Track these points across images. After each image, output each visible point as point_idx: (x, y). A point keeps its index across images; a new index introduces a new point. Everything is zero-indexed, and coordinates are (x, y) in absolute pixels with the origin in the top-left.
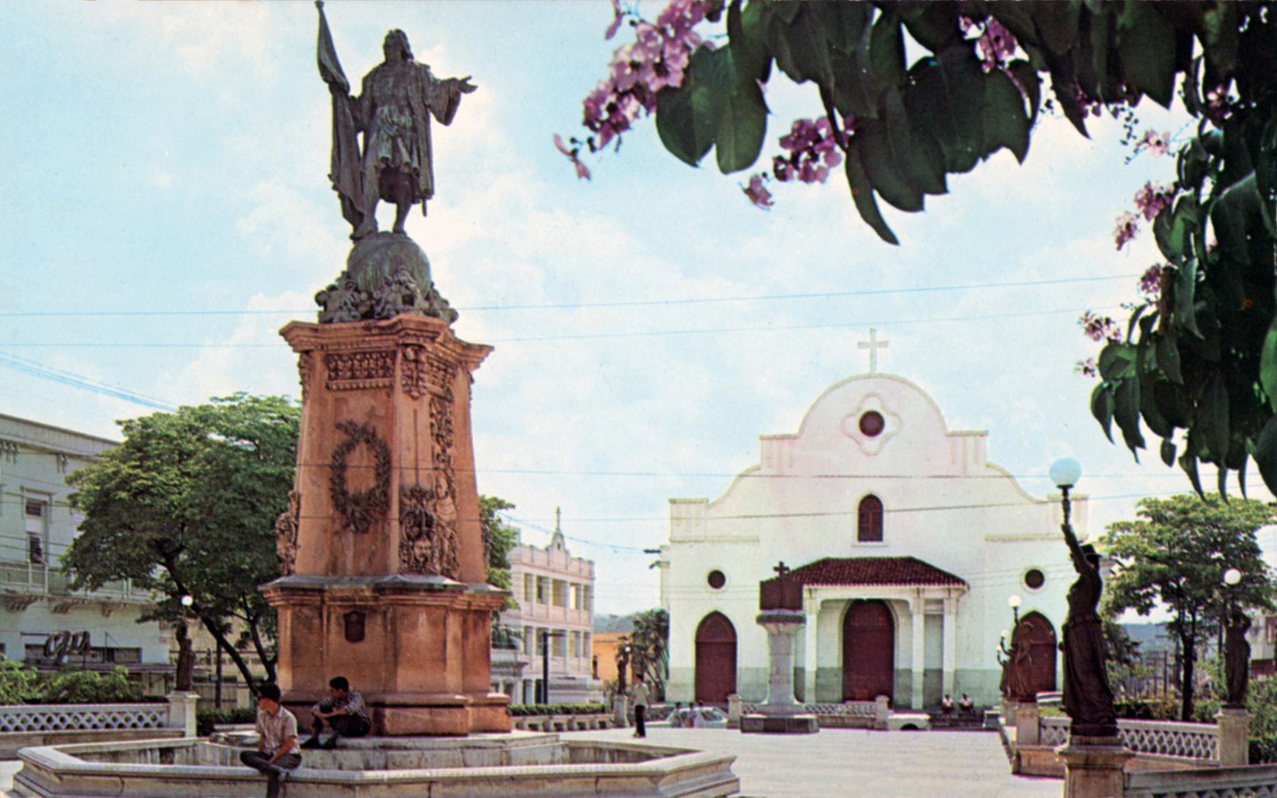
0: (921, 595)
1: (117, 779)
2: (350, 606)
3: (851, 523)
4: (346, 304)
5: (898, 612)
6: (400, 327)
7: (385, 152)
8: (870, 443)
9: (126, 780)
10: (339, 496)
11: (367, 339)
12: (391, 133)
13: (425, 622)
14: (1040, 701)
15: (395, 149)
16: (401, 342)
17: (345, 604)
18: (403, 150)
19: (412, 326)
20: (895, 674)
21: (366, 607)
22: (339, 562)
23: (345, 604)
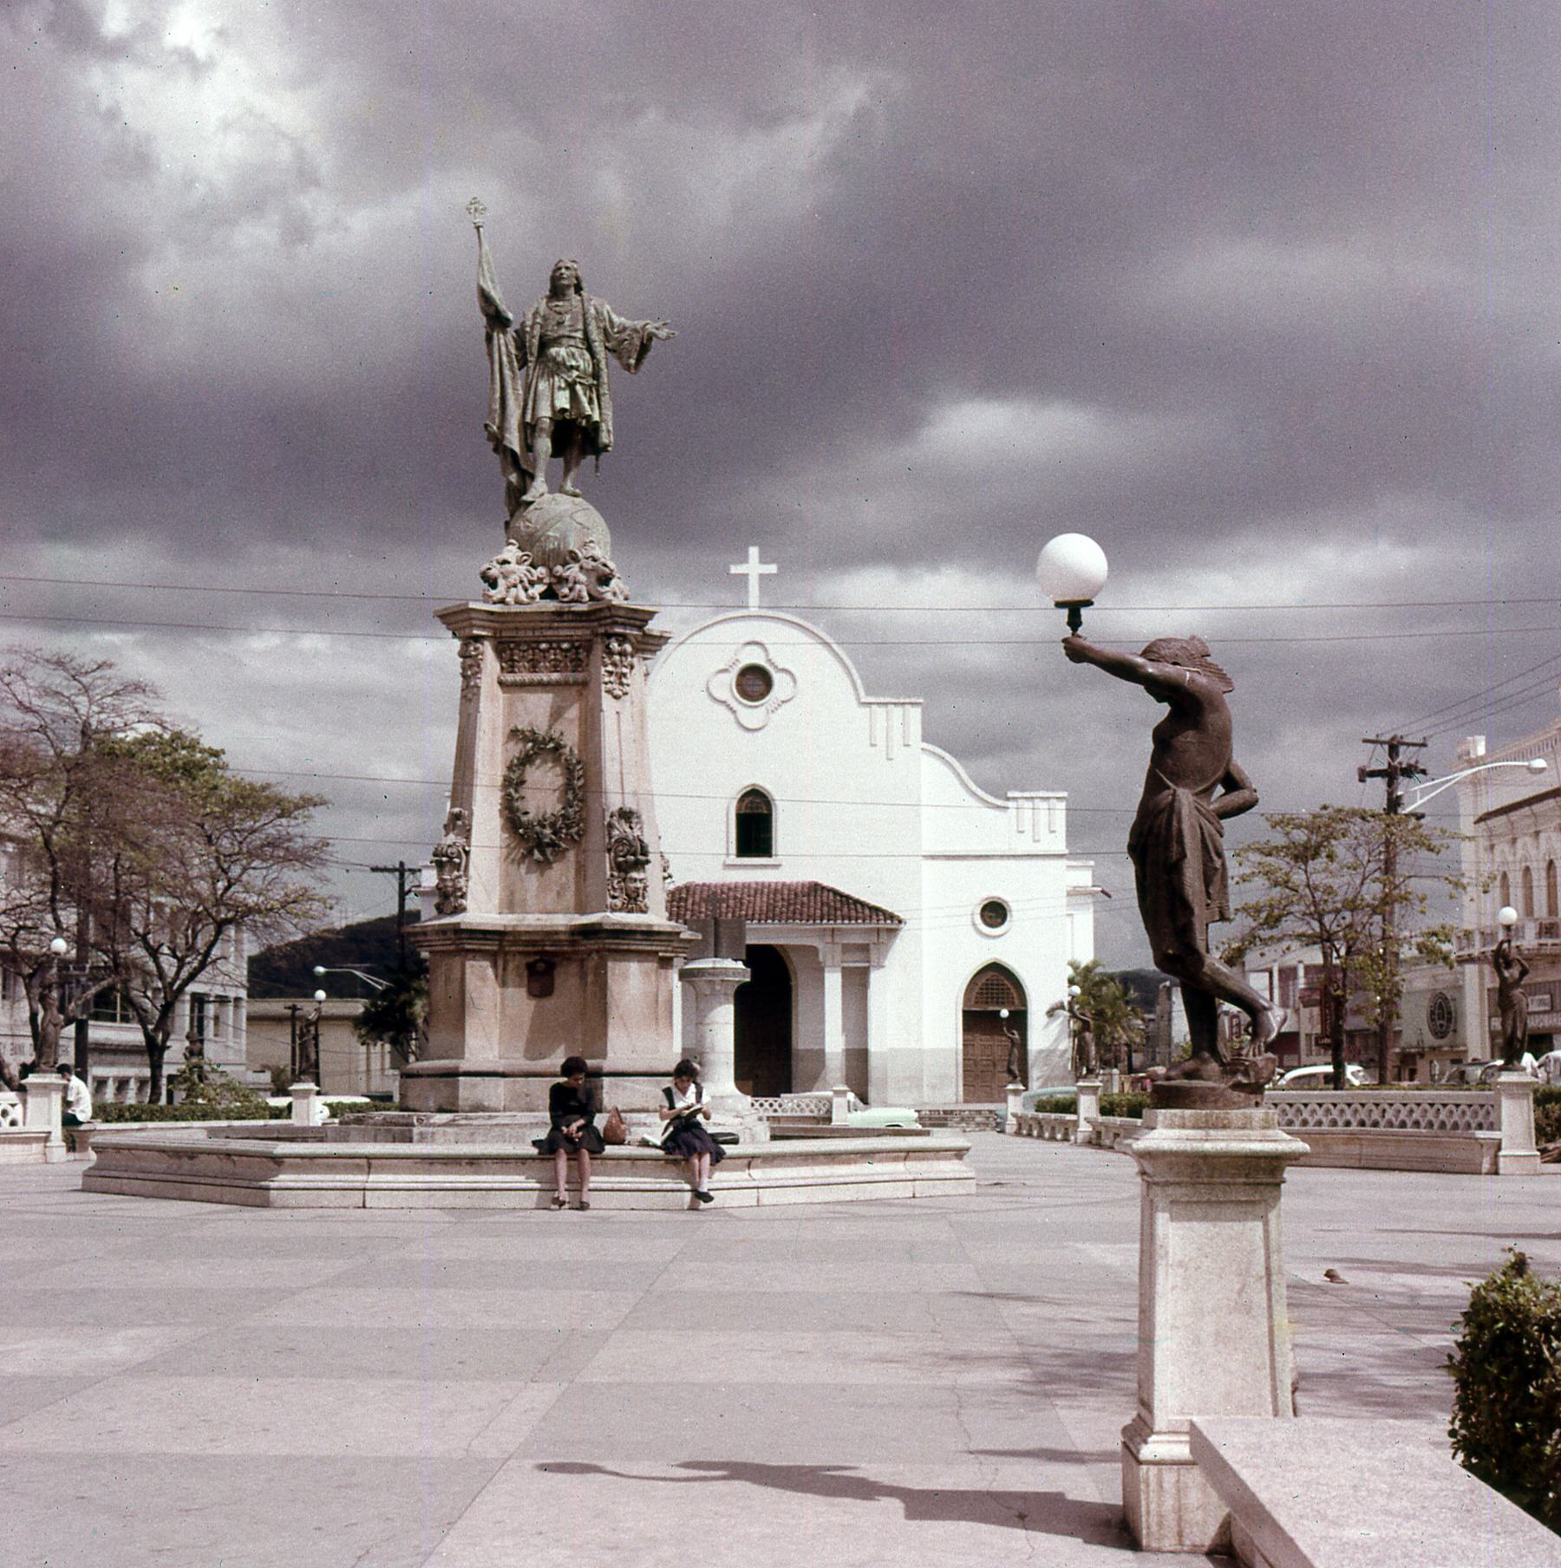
0: (837, 939)
1: (364, 1162)
2: (535, 953)
3: (725, 831)
4: (521, 582)
5: (797, 964)
6: (607, 614)
7: (563, 401)
8: (751, 714)
9: (373, 1161)
10: (512, 819)
11: (556, 625)
12: (570, 380)
13: (637, 973)
14: (1266, 1093)
15: (574, 397)
16: (602, 630)
17: (530, 949)
18: (584, 400)
19: (622, 613)
20: (794, 1057)
21: (554, 954)
22: (517, 896)
23: (530, 949)
